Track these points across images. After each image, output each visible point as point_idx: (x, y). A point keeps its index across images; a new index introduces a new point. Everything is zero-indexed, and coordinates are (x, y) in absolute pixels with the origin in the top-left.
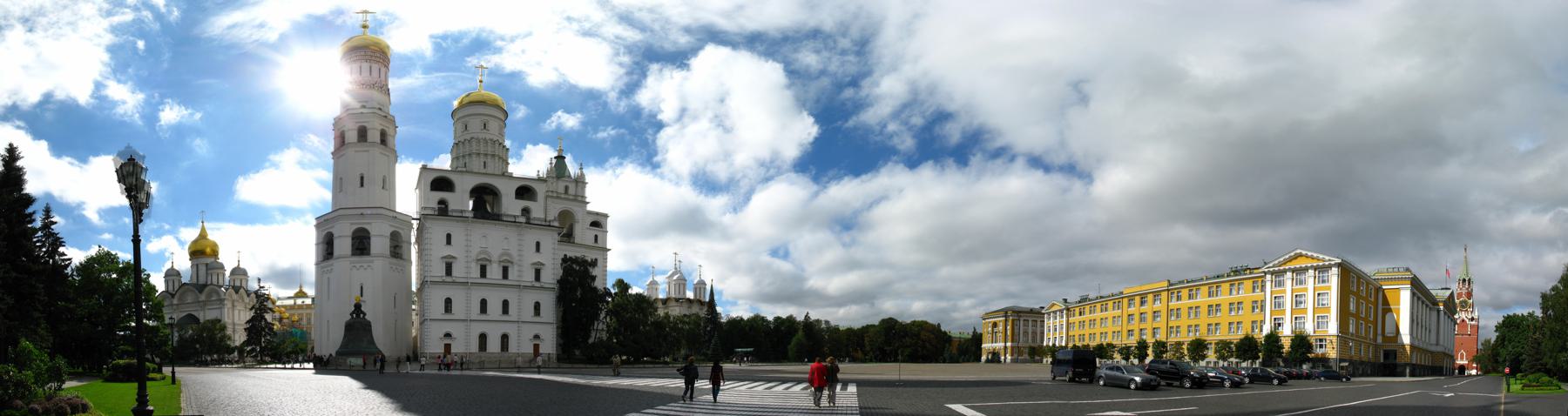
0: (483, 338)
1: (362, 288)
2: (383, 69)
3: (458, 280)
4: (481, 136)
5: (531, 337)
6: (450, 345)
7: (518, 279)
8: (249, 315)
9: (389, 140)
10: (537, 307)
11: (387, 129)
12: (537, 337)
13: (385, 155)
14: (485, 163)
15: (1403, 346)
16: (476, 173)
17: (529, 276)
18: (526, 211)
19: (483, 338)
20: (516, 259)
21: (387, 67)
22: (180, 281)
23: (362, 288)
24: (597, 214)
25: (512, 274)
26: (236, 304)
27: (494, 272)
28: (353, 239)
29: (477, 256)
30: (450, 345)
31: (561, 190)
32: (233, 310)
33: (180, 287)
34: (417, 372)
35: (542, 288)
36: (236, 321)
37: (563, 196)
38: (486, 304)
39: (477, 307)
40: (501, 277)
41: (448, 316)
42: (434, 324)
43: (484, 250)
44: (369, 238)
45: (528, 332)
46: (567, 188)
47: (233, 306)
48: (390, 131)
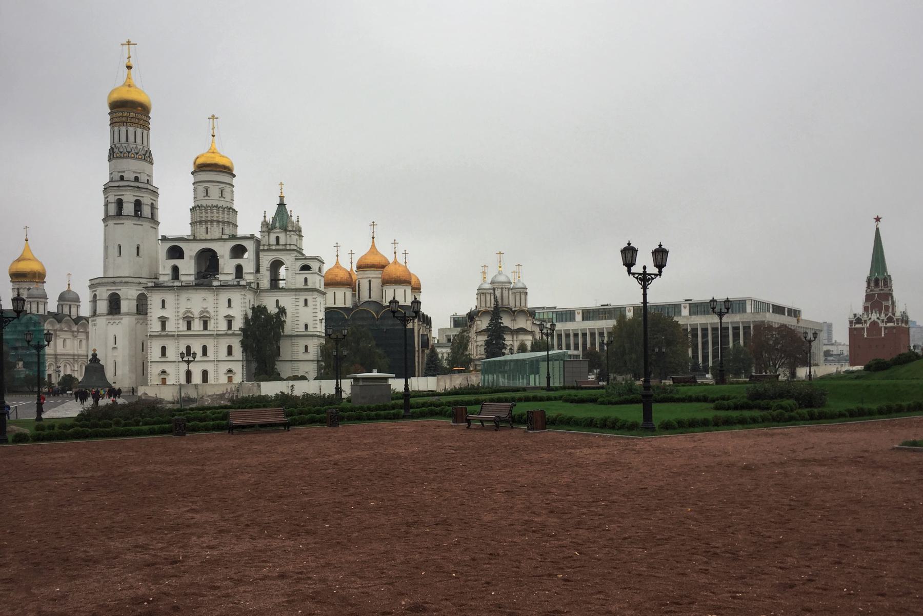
3: (170, 333)
4: (204, 203)
5: (225, 371)
6: (165, 378)
7: (176, 330)
10: (230, 349)
12: (230, 371)
14: (223, 228)
15: (711, 374)
16: (209, 240)
17: (223, 326)
18: (175, 269)
20: (212, 314)
24: (106, 248)
25: (211, 326)
27: (197, 326)
29: (184, 315)
30: (165, 378)
31: (273, 241)
34: (22, 403)
35: (167, 336)
37: (274, 247)
39: (225, 351)
40: (202, 328)
41: (163, 359)
42: (154, 366)
43: (189, 311)
45: (224, 367)
46: (278, 238)
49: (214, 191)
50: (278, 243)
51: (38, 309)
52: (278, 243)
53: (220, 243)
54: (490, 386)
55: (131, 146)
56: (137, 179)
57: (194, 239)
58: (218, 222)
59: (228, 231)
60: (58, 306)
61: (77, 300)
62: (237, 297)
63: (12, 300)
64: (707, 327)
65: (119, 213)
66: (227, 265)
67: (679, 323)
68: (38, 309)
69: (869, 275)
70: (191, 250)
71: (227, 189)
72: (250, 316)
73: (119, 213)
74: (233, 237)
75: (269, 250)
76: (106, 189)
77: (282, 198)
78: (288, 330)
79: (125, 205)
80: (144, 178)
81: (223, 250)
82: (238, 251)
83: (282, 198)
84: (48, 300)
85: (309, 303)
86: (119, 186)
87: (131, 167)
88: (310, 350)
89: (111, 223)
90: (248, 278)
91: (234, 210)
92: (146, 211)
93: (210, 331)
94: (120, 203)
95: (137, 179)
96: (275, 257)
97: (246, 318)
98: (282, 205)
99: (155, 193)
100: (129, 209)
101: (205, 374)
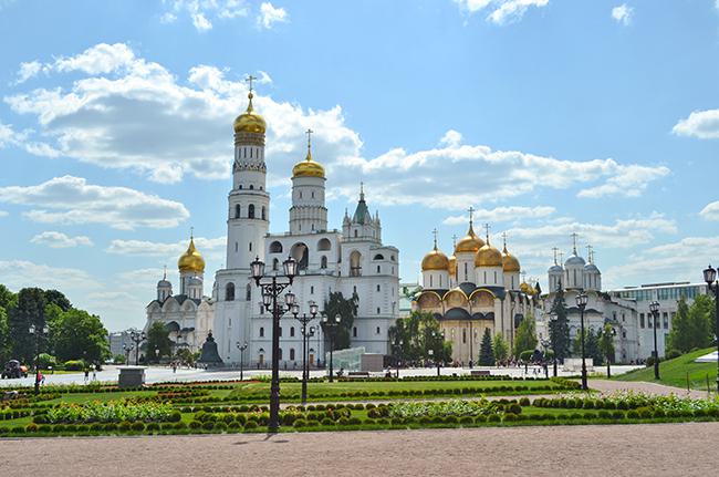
49: (307, 193)
50: (356, 236)
52: (356, 236)
53: (310, 238)
56: (252, 187)
57: (290, 235)
58: (309, 219)
59: (318, 227)
61: (169, 285)
62: (317, 283)
65: (238, 217)
66: (315, 257)
67: (143, 61)
69: (224, 433)
70: (287, 245)
71: (318, 191)
72: (328, 300)
73: (238, 217)
74: (323, 232)
76: (231, 196)
77: (362, 195)
78: (361, 312)
79: (241, 210)
80: (257, 186)
81: (312, 244)
82: (324, 244)
83: (362, 195)
85: (381, 288)
87: (248, 177)
88: (381, 331)
89: (231, 223)
90: (331, 267)
91: (323, 208)
92: (258, 213)
94: (238, 208)
95: (252, 187)
97: (326, 304)
98: (362, 202)
99: (267, 197)
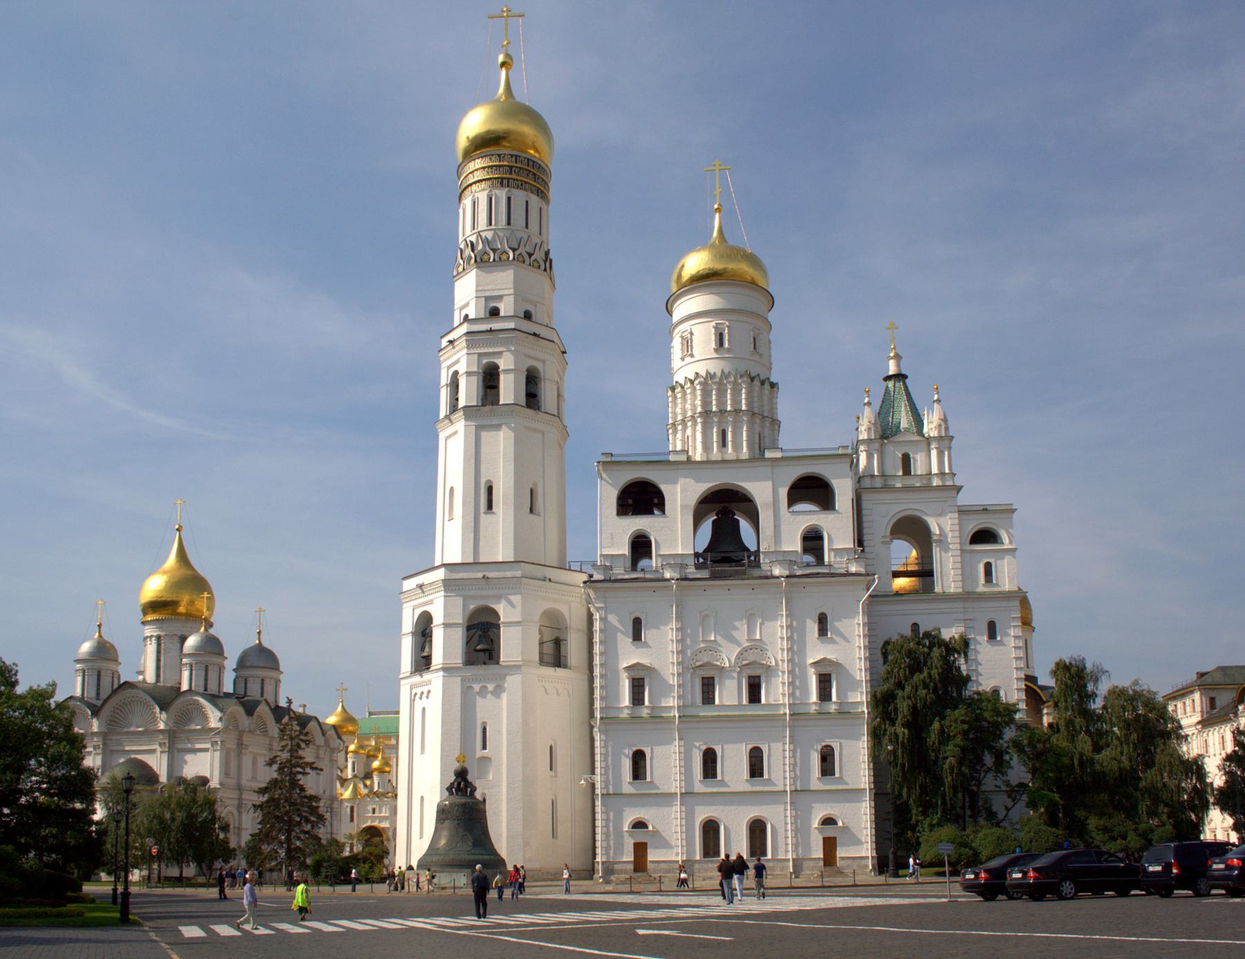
0: (711, 830)
1: (527, 202)
2: (534, 200)
8: (268, 774)
9: (547, 394)
11: (539, 366)
13: (535, 430)
19: (711, 830)
21: (542, 194)
22: (115, 674)
23: (527, 202)
26: (246, 739)
27: (729, 694)
28: (469, 628)
32: (240, 754)
33: (114, 692)
36: (244, 782)
38: (714, 761)
44: (498, 627)
45: (745, 815)
47: (240, 745)
48: (548, 372)
51: (262, 689)
54: (735, 877)
55: (519, 235)
60: (235, 681)
63: (1057, 664)
64: (469, 378)
68: (262, 689)
75: (887, 488)
84: (120, 666)
86: (491, 331)
93: (722, 706)
96: (903, 507)
100: (509, 389)
101: (757, 830)
